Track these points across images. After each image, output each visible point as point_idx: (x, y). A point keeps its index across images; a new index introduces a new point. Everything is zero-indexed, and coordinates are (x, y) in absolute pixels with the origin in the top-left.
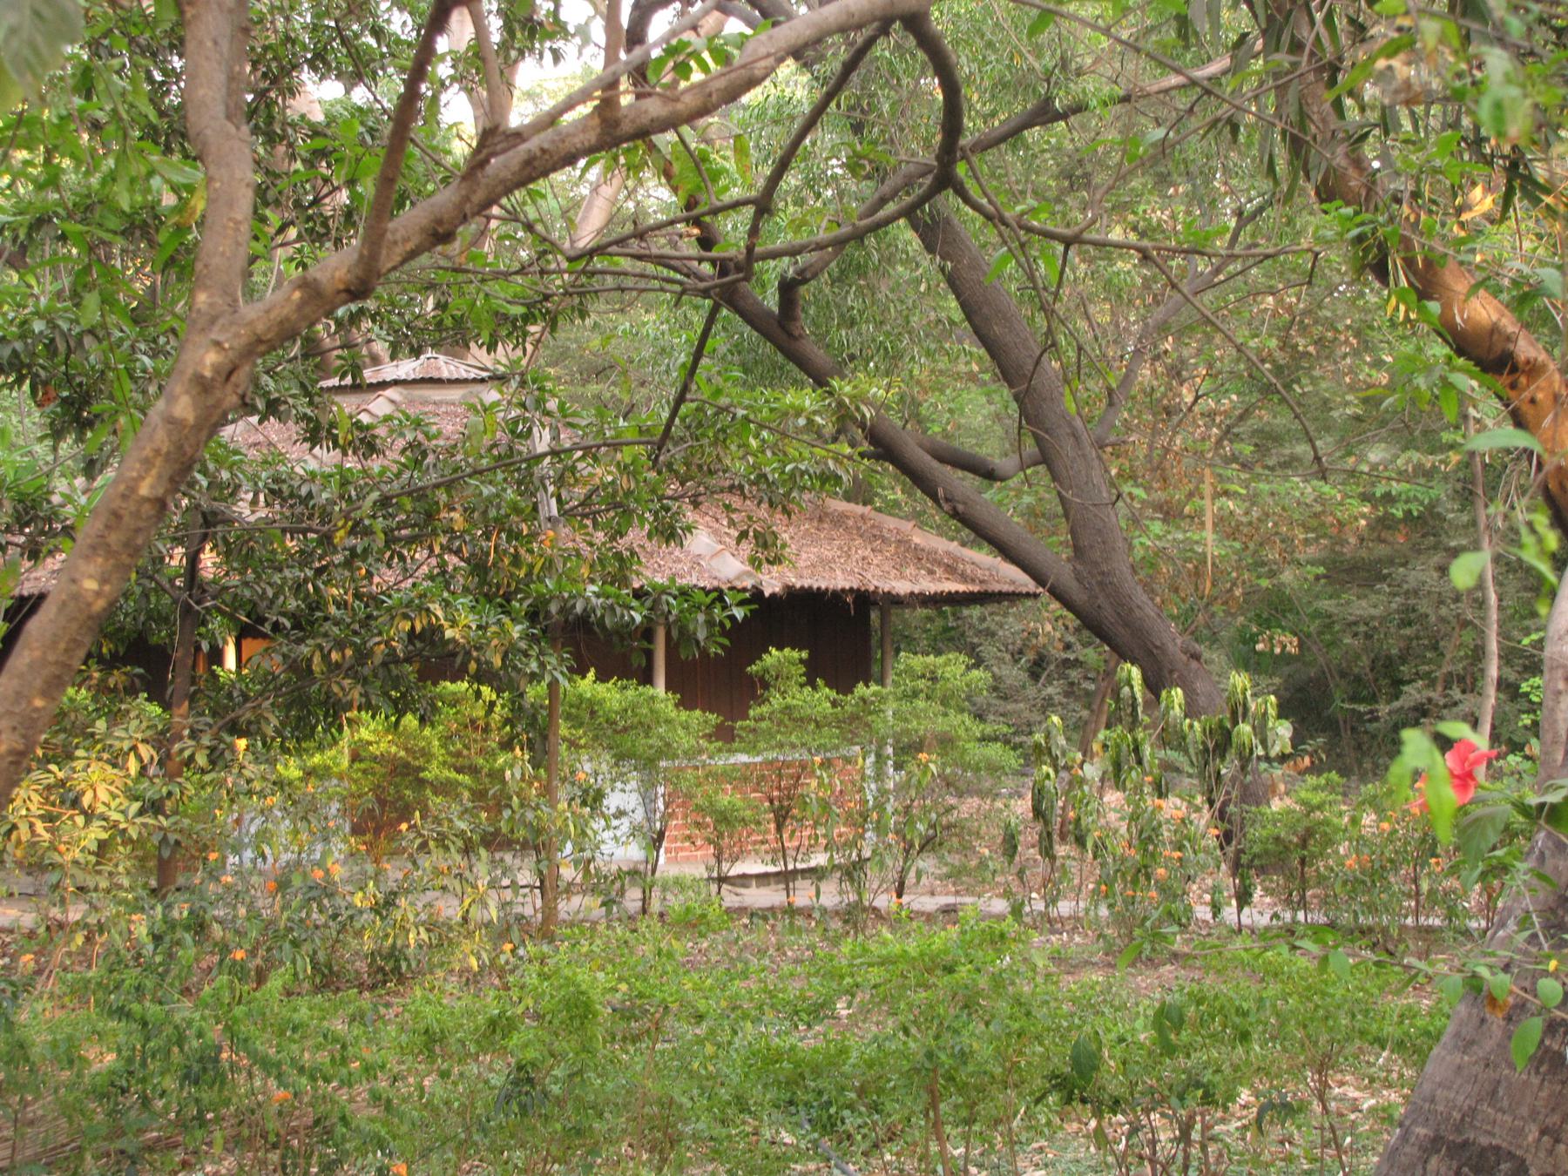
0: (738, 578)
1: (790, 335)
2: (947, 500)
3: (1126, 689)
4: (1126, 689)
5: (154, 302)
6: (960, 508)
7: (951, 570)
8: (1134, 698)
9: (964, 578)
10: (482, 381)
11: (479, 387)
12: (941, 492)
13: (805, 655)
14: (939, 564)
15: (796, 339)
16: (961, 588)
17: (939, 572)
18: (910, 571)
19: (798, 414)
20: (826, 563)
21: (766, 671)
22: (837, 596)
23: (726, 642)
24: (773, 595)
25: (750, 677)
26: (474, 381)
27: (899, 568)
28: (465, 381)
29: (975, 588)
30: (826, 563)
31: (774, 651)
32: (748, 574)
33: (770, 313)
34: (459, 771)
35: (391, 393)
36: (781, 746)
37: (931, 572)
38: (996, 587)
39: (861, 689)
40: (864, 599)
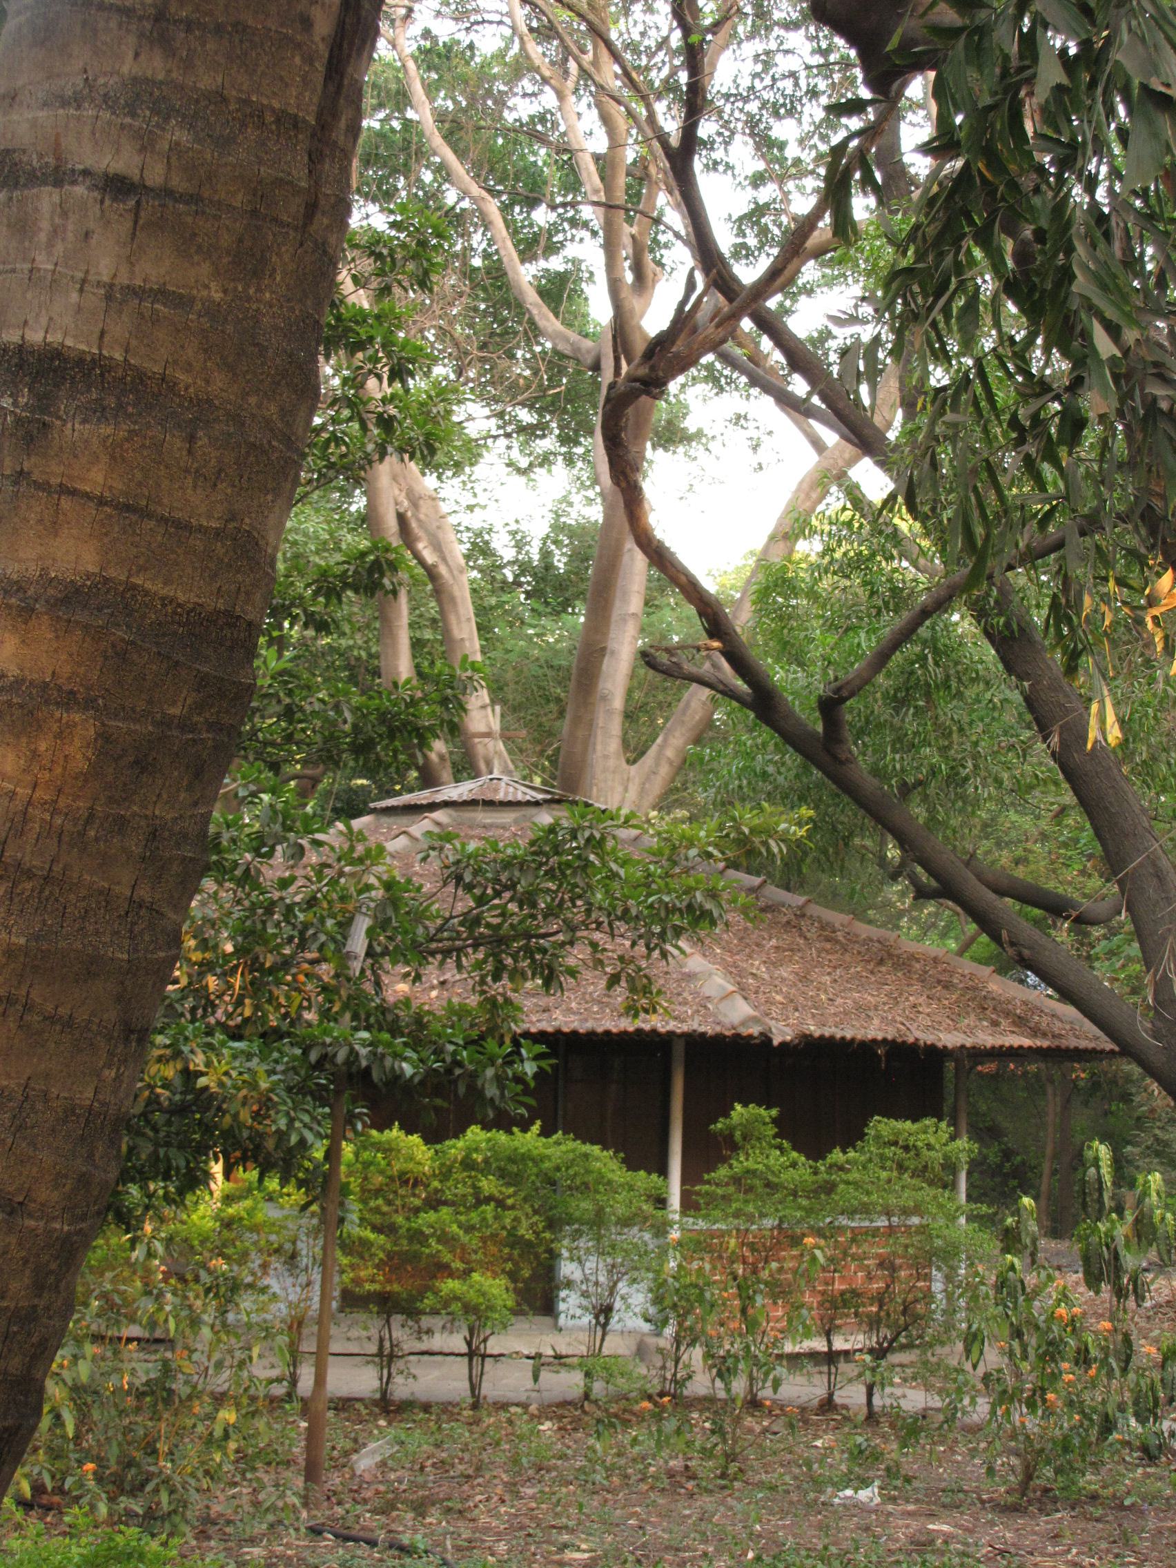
0: (743, 1023)
1: (835, 758)
2: (1012, 944)
3: (1092, 1170)
4: (1092, 1170)
5: (828, 751)
6: (1026, 952)
7: (1020, 1022)
8: (1099, 1180)
9: (1035, 1032)
10: (537, 804)
11: (532, 811)
12: (1004, 933)
13: (774, 1112)
14: (1007, 1014)
15: (842, 763)
16: (1027, 1042)
17: (1004, 1023)
18: (970, 1020)
19: (691, 845)
20: (862, 1010)
21: (732, 1129)
22: (867, 1047)
23: (532, 1101)
24: (784, 1045)
25: (714, 1135)
26: (528, 803)
27: (955, 1017)
28: (518, 804)
29: (1045, 1044)
30: (862, 1010)
31: (738, 1107)
32: (754, 1020)
33: (814, 734)
34: (376, 1229)
35: (439, 815)
36: (737, 1215)
37: (995, 1024)
38: (1072, 1043)
39: (837, 1156)
40: (936, 1055)
